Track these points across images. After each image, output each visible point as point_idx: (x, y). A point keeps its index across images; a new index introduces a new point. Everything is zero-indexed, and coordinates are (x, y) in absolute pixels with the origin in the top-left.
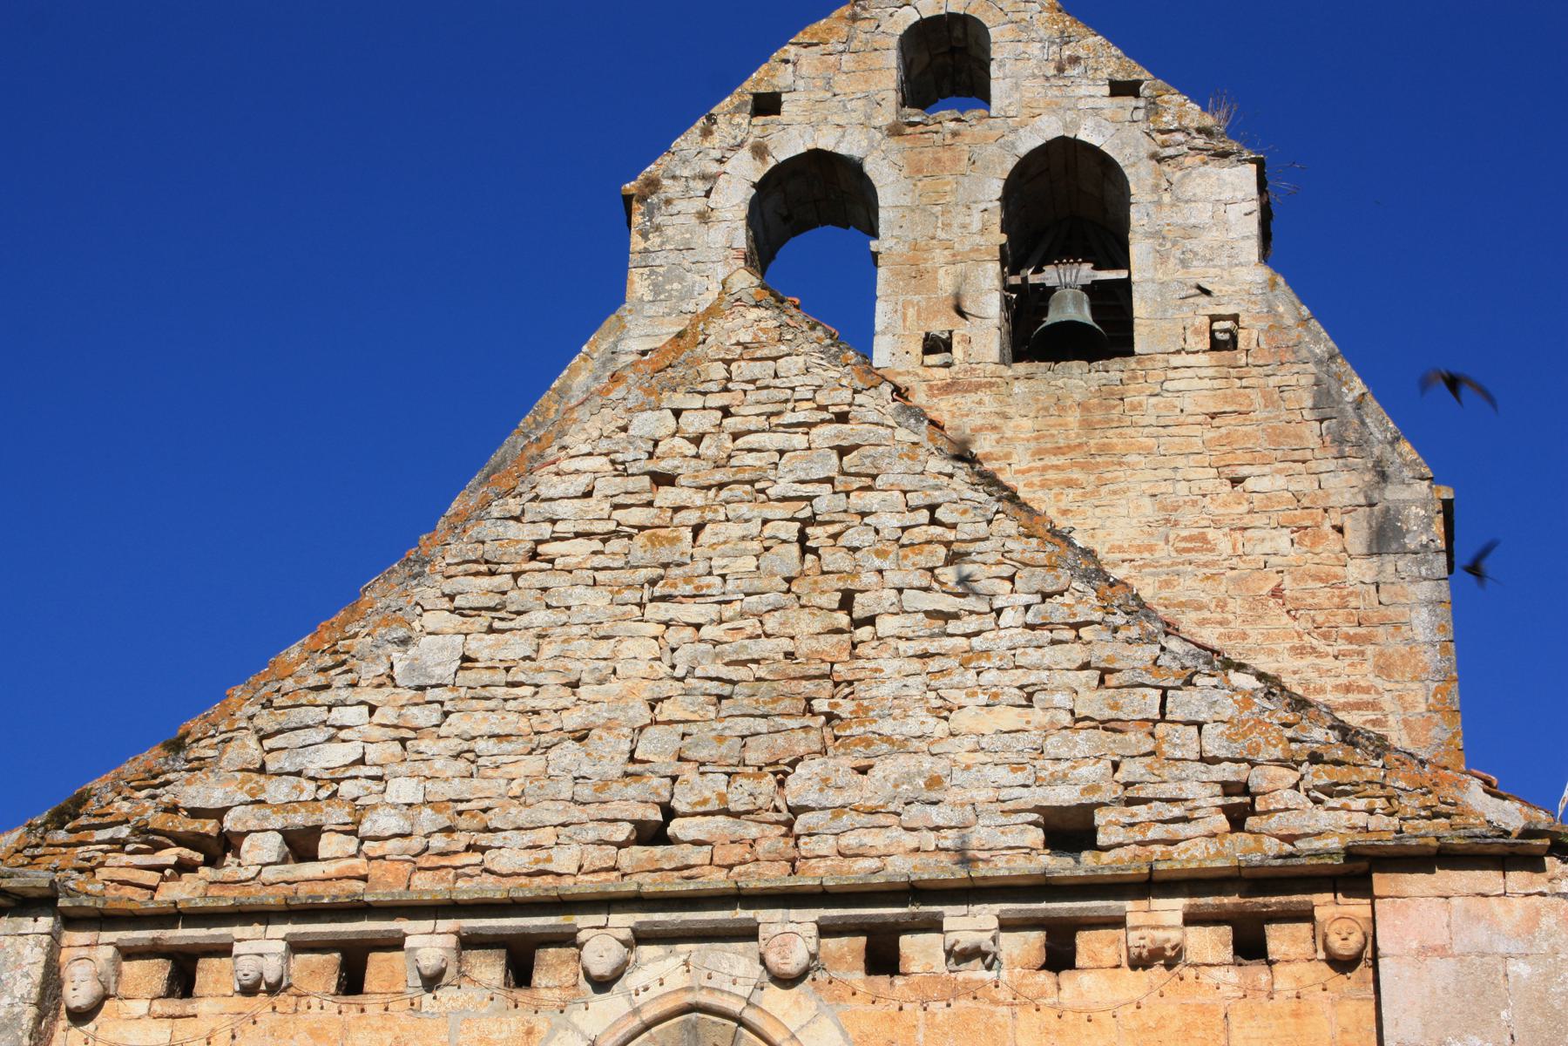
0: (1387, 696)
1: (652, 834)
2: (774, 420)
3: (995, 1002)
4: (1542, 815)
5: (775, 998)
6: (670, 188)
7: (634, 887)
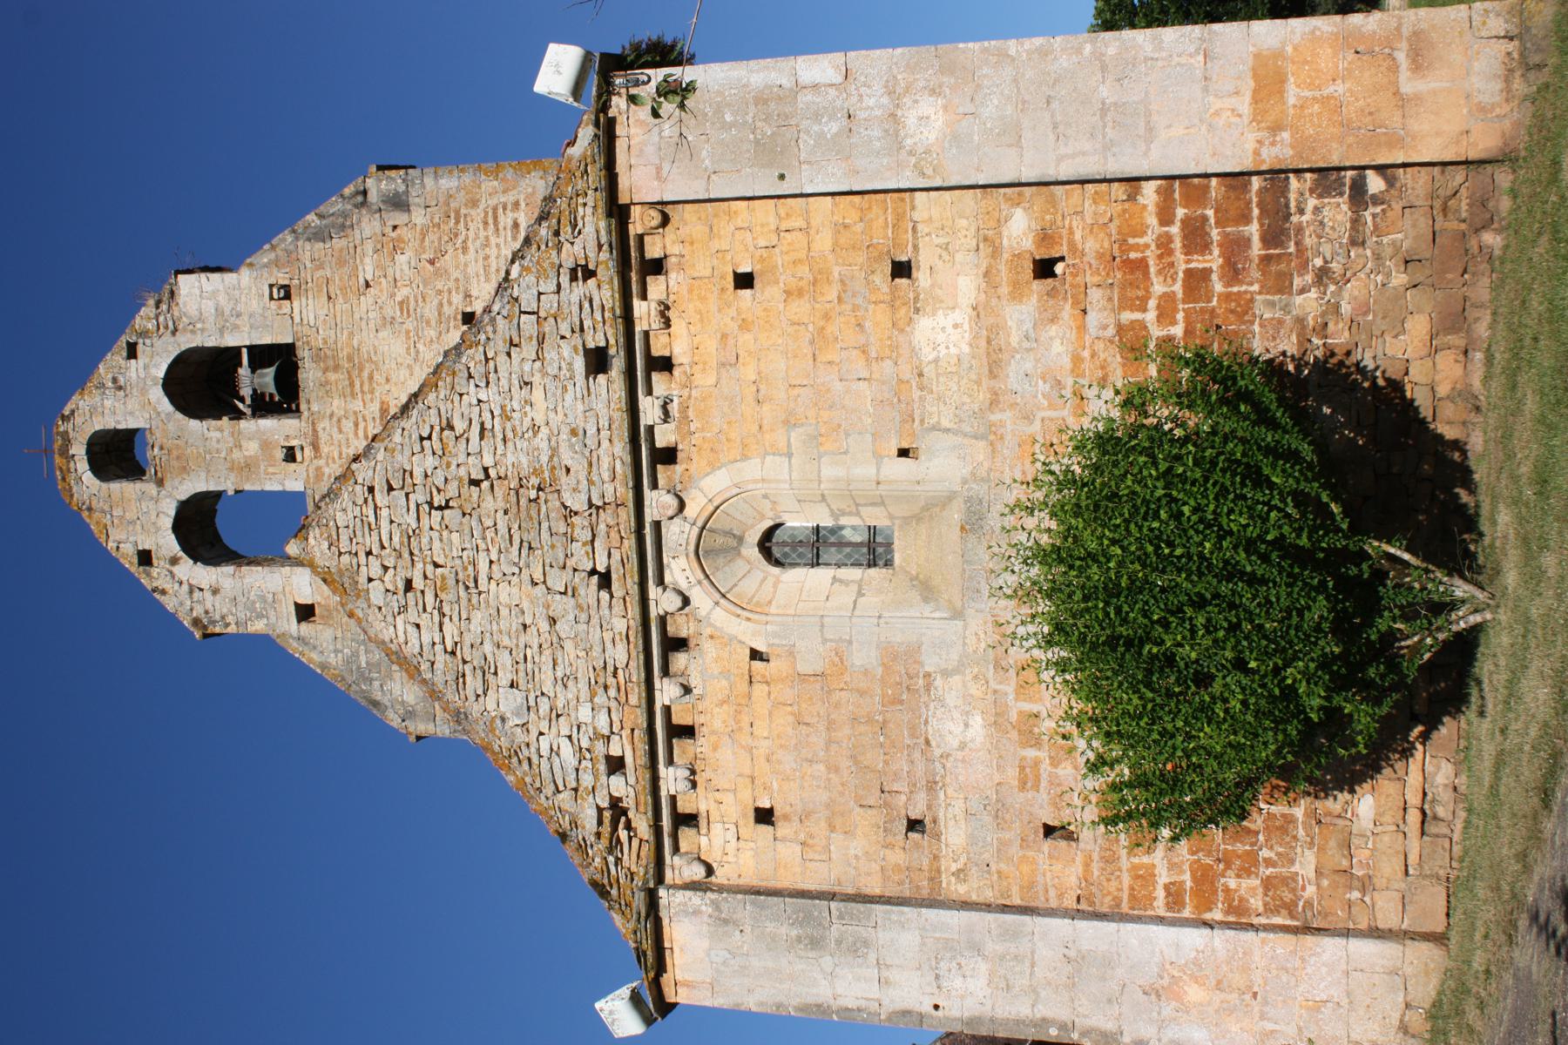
0: (489, 202)
1: (605, 581)
2: (373, 526)
3: (690, 397)
4: (585, 117)
5: (691, 511)
6: (198, 611)
7: (636, 587)
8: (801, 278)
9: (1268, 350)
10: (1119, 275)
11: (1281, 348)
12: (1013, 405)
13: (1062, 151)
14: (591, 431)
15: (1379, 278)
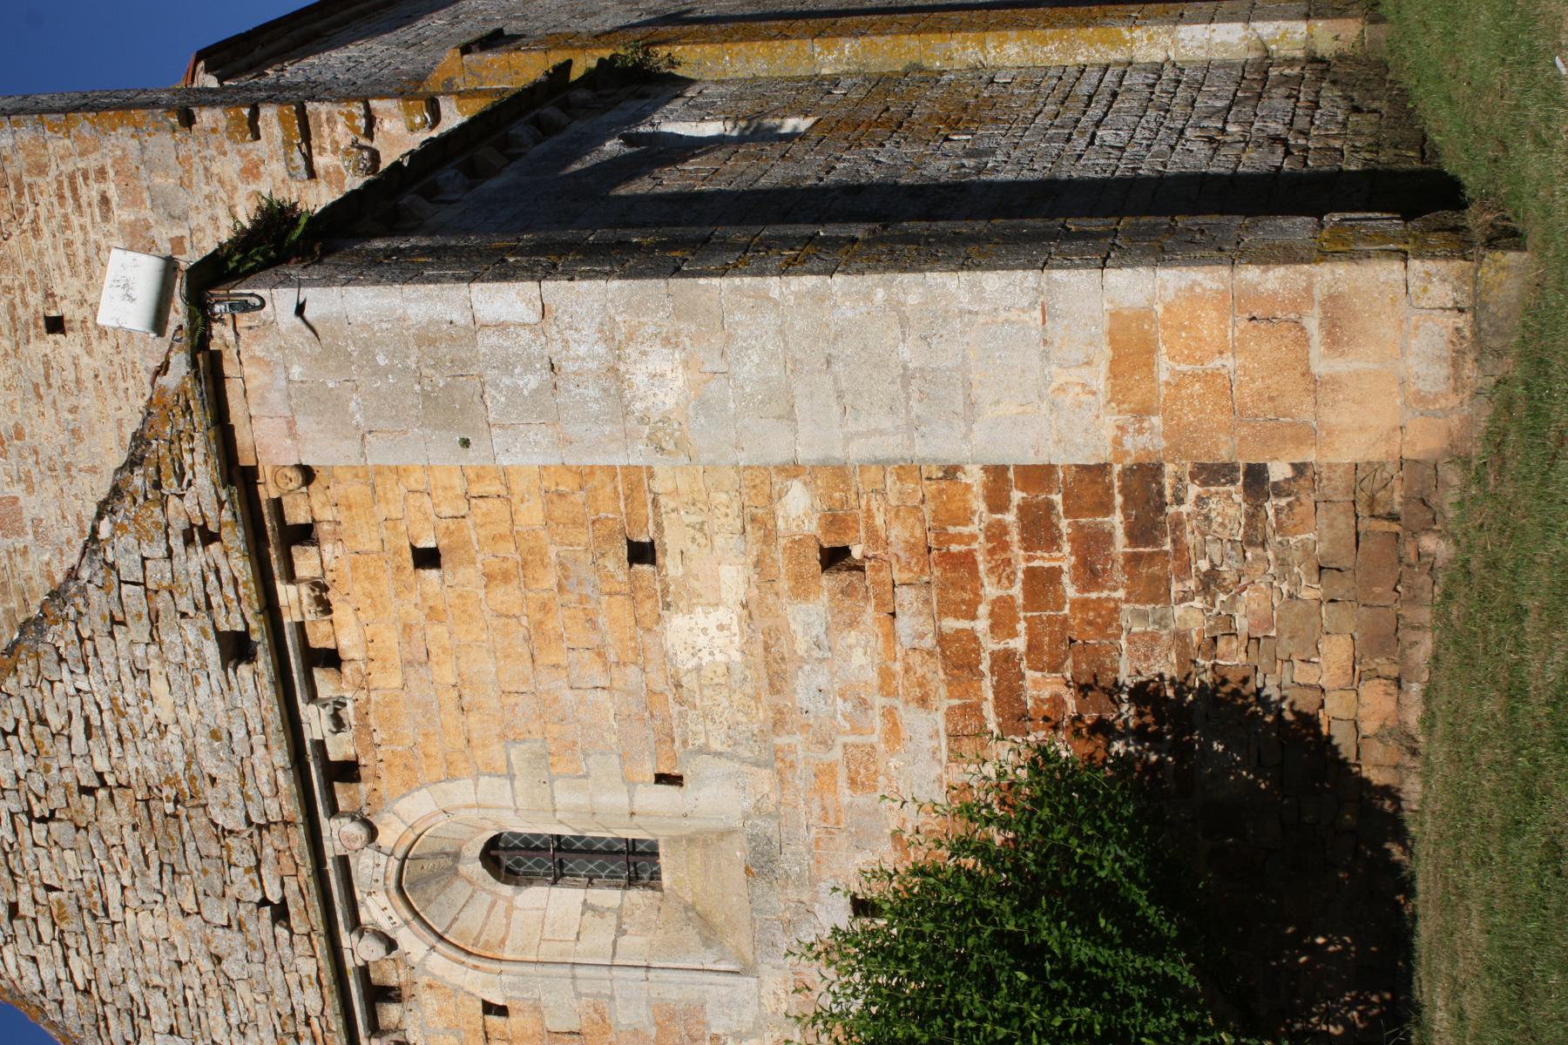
0: (62, 168)
1: (281, 913)
3: (368, 701)
5: (386, 838)
8: (505, 559)
9: (1139, 673)
10: (937, 572)
11: (1156, 669)
12: (805, 727)
13: (852, 427)
14: (239, 734)
15: (1285, 587)
